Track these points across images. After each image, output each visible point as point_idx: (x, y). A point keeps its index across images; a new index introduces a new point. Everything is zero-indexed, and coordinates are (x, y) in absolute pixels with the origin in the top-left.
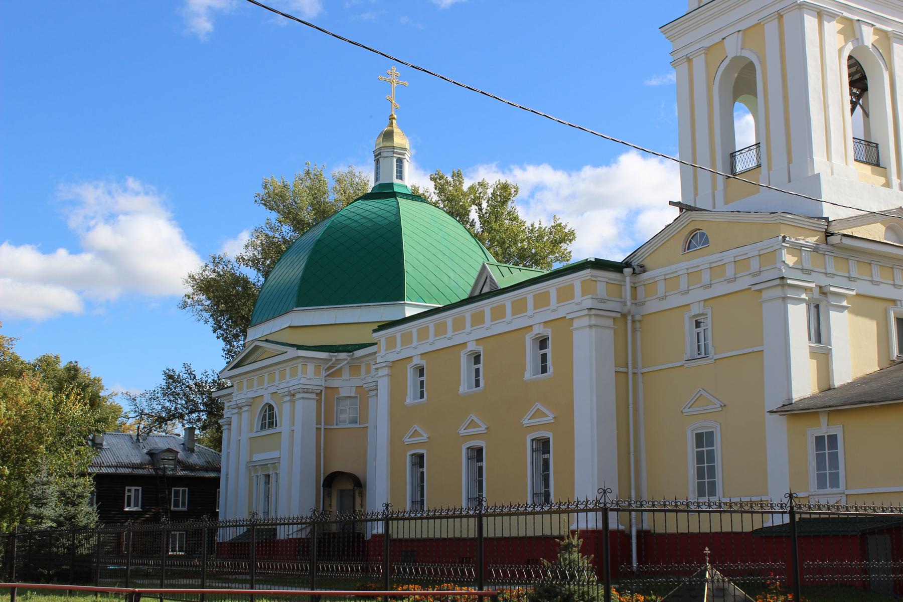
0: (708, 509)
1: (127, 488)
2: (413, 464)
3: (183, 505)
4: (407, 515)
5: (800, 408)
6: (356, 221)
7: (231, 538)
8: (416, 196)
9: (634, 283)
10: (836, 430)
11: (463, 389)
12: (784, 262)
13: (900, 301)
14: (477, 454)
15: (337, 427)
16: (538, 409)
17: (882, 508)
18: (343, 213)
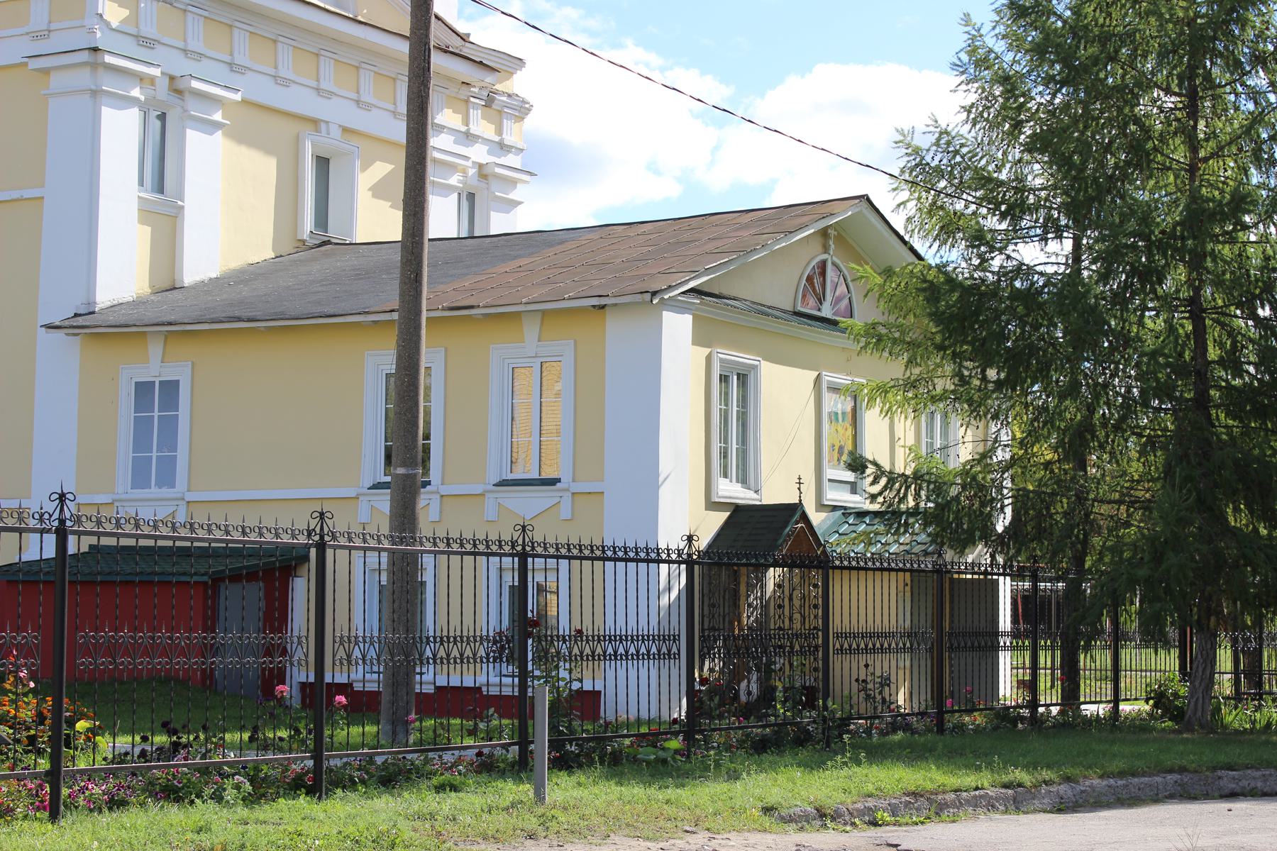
0: (17, 525)
5: (108, 323)
12: (101, 16)
13: (327, 122)
17: (243, 528)
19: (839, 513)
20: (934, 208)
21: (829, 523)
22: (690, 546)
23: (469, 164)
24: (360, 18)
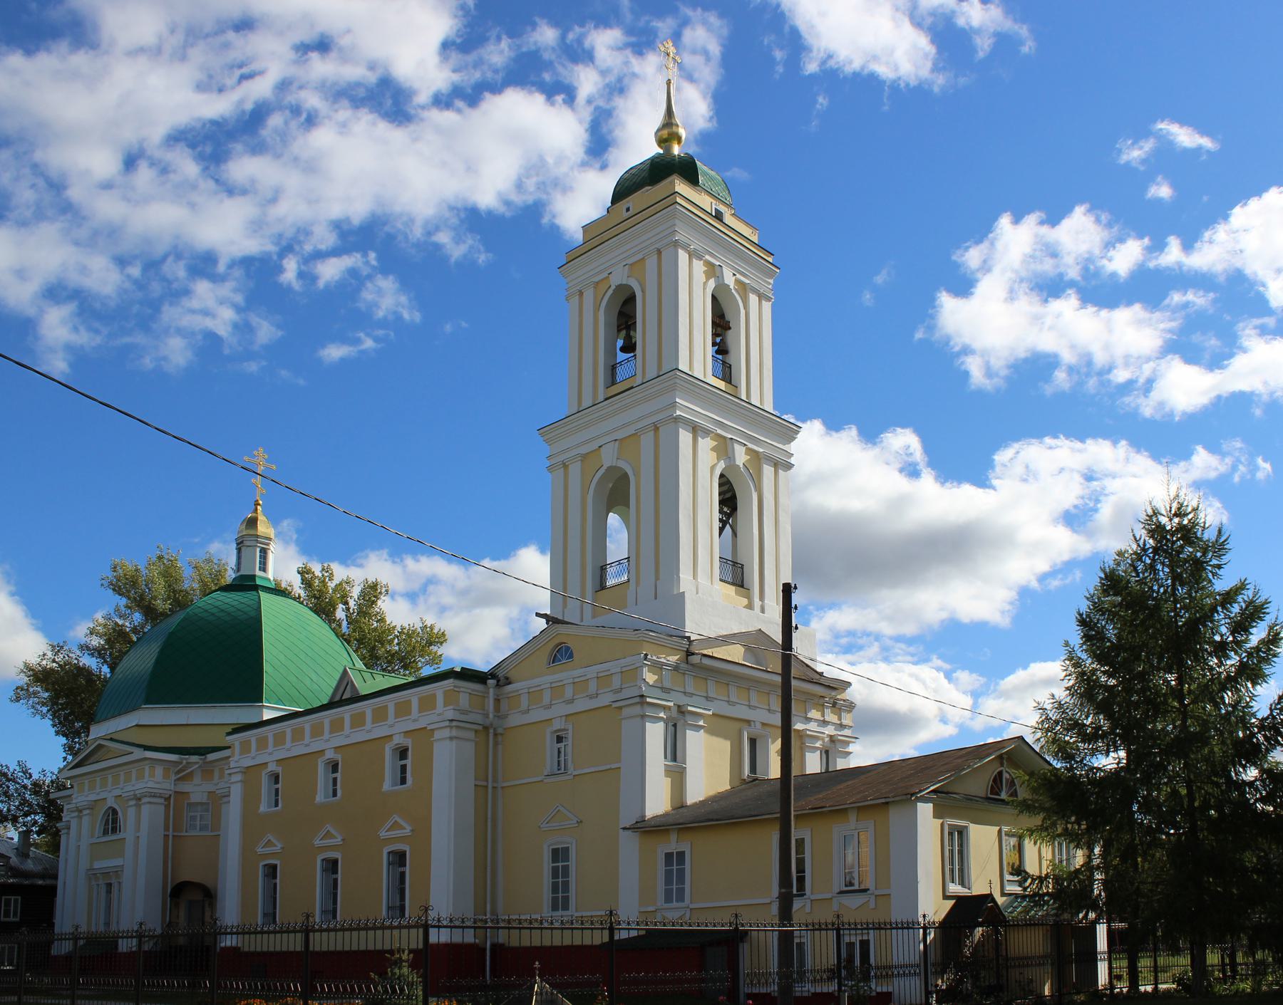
3: (15, 915)
6: (213, 614)
7: (67, 951)
8: (279, 591)
9: (498, 696)
10: (685, 847)
11: (320, 798)
12: (645, 680)
13: (754, 721)
14: (331, 866)
15: (187, 834)
16: (396, 821)
17: (698, 923)
18: (201, 604)
19: (1013, 897)
20: (1054, 741)
21: (1007, 902)
23: (825, 736)
24: (769, 670)
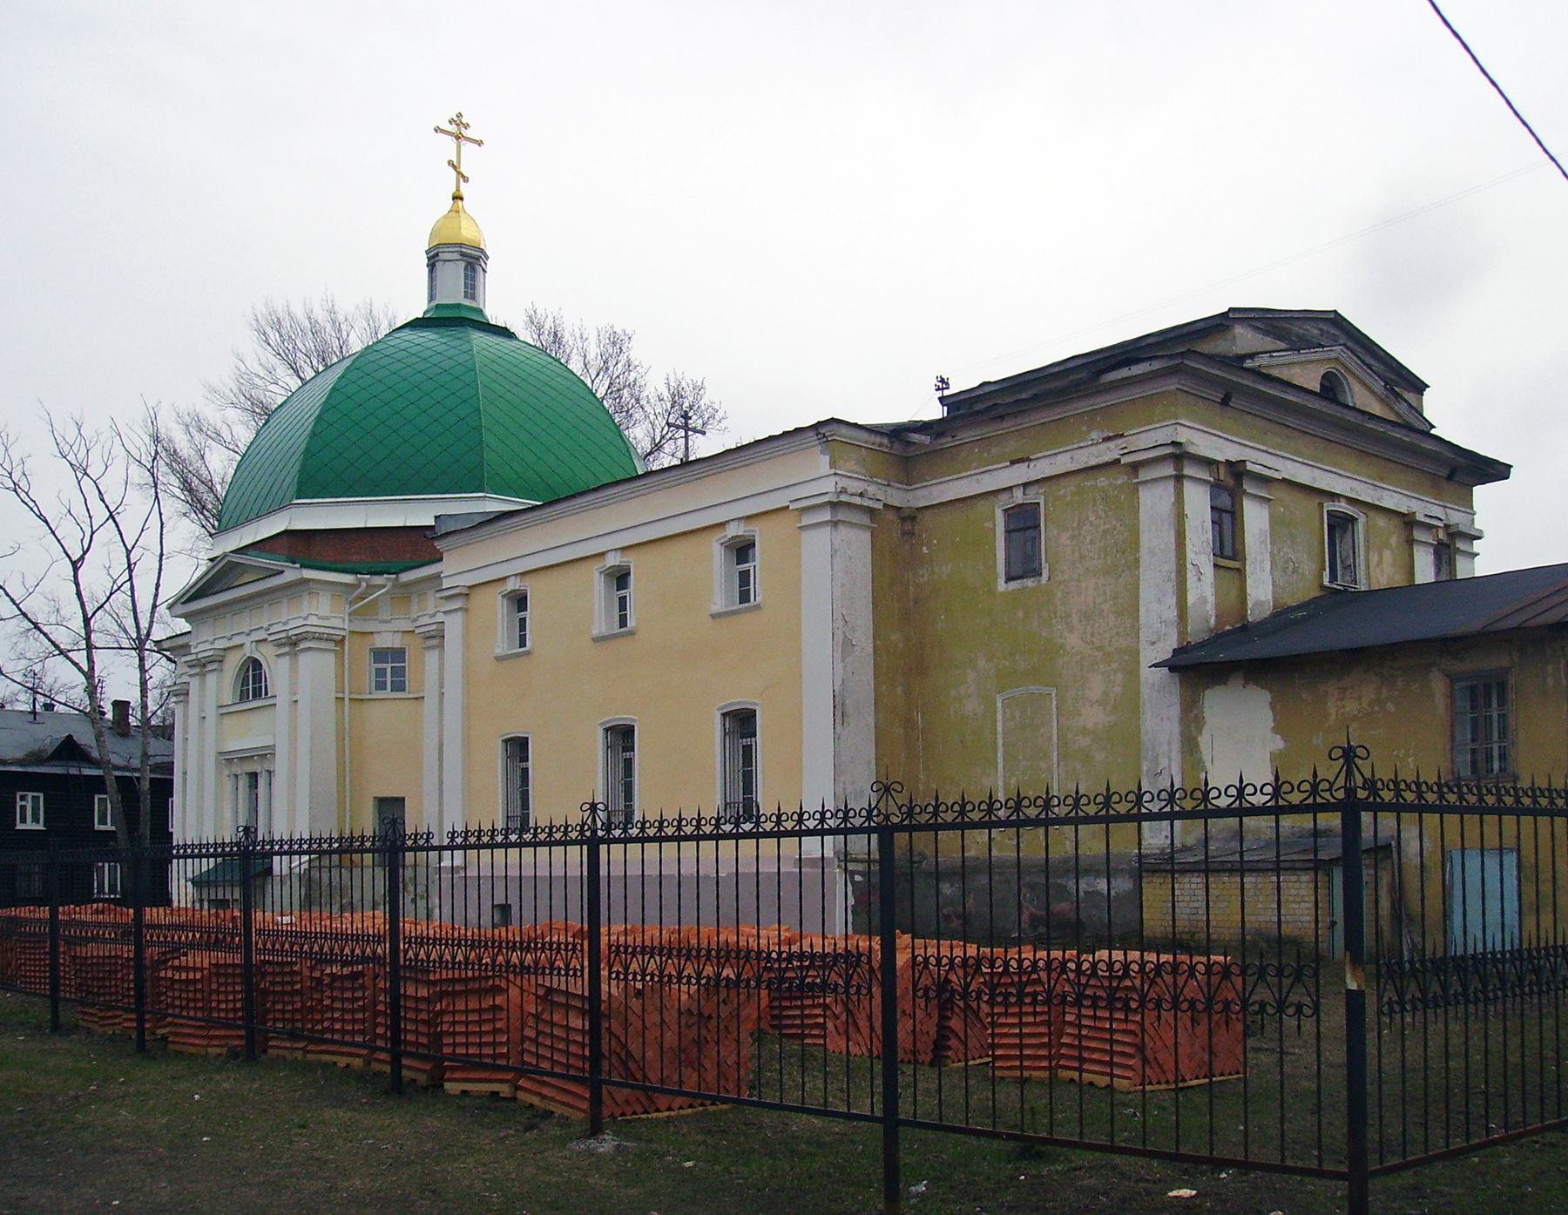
1: (19, 794)
2: (509, 757)
4: (297, 846)
22: (1349, 773)
